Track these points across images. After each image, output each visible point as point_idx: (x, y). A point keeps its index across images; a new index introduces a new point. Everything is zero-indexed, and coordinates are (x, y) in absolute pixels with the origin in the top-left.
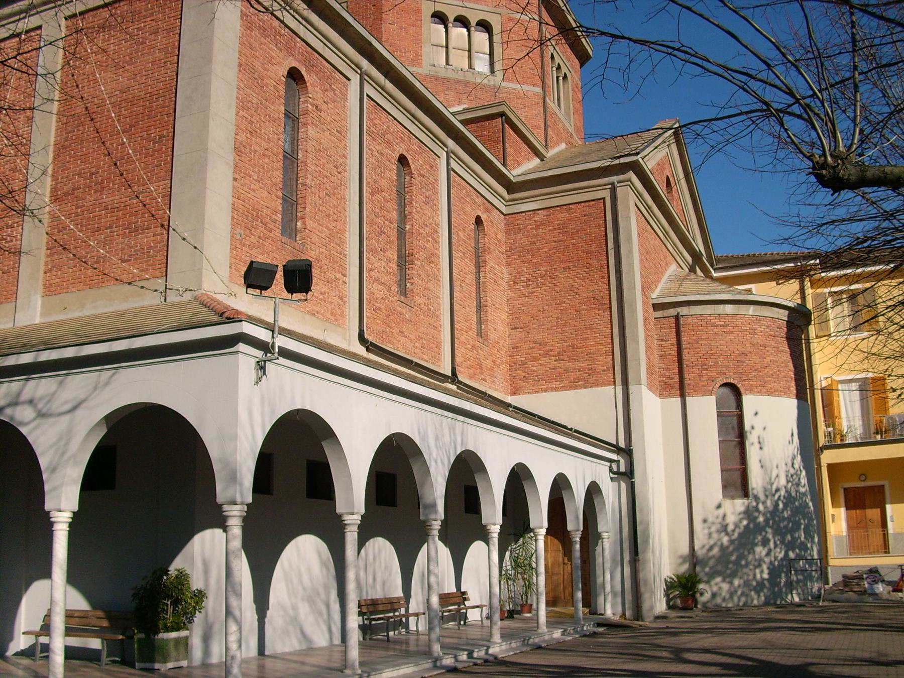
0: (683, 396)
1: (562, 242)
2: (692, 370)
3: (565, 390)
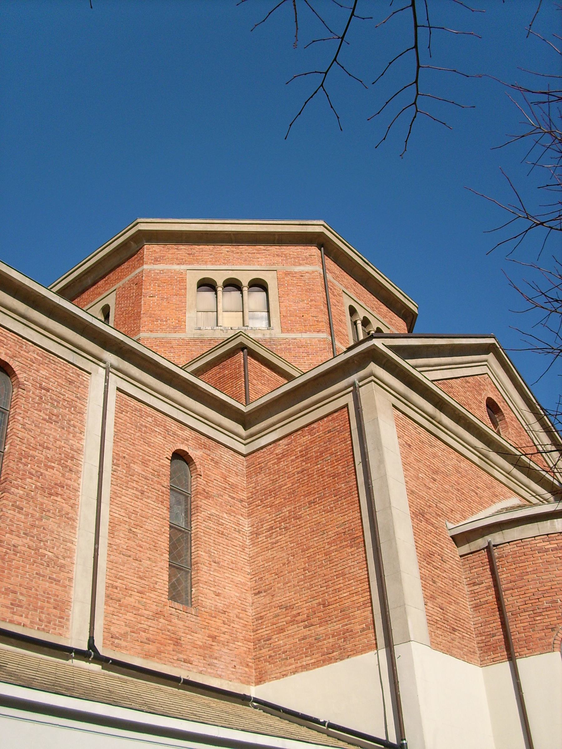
0: (511, 658)
1: (305, 472)
2: (520, 618)
3: (318, 667)
